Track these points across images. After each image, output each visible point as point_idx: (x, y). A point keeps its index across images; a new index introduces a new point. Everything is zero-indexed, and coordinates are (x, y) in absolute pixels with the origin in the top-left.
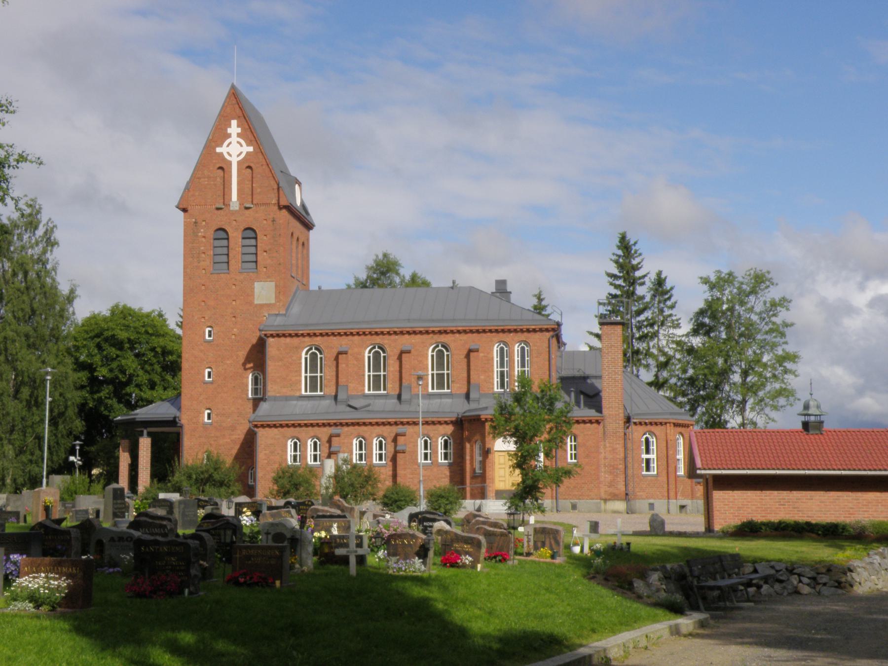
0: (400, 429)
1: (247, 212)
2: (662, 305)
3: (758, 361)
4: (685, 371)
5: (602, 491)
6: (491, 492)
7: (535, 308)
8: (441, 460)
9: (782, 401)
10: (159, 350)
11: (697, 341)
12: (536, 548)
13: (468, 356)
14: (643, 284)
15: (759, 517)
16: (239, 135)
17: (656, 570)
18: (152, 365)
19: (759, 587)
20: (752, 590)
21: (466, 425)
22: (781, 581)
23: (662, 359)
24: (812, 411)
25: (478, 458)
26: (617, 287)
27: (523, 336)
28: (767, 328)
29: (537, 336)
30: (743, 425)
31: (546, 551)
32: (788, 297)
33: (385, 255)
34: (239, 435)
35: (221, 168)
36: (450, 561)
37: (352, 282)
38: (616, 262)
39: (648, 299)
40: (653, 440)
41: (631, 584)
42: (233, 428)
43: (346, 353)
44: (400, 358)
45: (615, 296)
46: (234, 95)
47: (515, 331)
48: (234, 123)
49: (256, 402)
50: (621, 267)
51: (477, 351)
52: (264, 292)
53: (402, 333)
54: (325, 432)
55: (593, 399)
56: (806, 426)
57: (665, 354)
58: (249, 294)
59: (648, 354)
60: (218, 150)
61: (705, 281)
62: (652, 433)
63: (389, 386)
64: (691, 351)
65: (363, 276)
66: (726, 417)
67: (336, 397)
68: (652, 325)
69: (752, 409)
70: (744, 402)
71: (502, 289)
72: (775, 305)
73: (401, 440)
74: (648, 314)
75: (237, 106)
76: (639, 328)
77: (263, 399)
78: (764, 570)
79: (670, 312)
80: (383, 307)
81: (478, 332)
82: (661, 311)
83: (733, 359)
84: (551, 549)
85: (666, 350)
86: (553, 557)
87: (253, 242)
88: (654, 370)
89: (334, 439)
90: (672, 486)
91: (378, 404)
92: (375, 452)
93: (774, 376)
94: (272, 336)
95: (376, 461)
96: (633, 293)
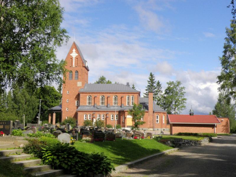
0: (107, 113)
1: (76, 68)
2: (159, 88)
3: (178, 100)
4: (163, 102)
5: (148, 126)
6: (126, 126)
7: (132, 88)
8: (116, 119)
9: (183, 108)
10: (54, 95)
11: (165, 95)
12: (147, 136)
13: (121, 98)
14: (155, 83)
15: (182, 132)
16: (75, 52)
17: (169, 140)
18: (53, 98)
19: (185, 144)
20: (184, 145)
21: (121, 112)
22: (189, 143)
23: (159, 99)
24: (192, 111)
25: (123, 119)
26: (149, 84)
27: (133, 94)
28: (180, 93)
29: (136, 94)
30: (175, 113)
31: (149, 137)
32: (185, 87)
33: (103, 76)
34: (74, 113)
35: (71, 58)
36: (135, 138)
37: (96, 82)
38: (150, 79)
39: (156, 86)
40: (158, 116)
41: (165, 143)
42: (72, 112)
43: (96, 97)
44: (107, 98)
45: (149, 86)
46: (74, 43)
47: (131, 93)
48: (74, 49)
49: (77, 107)
50: (150, 80)
51: (123, 97)
52: (79, 84)
53: (108, 93)
54: (92, 113)
55: (147, 107)
56: (190, 114)
57: (159, 98)
58: (76, 85)
59: (156, 98)
60: (71, 55)
61: (168, 83)
62: (158, 115)
63: (105, 104)
64: (164, 97)
65: (98, 81)
66: (171, 111)
67: (94, 106)
68: (157, 92)
69: (177, 110)
70: (175, 108)
71: (128, 84)
72: (182, 88)
73: (107, 115)
74: (156, 90)
75: (75, 46)
76: (59, 77)
77: (79, 106)
78: (186, 141)
79: (161, 89)
80: (102, 87)
81: (123, 93)
82: (159, 89)
83: (173, 99)
84: (150, 136)
85: (160, 97)
86: (150, 138)
87: (77, 74)
88: (157, 101)
89: (94, 115)
90: (162, 125)
91: (103, 108)
92: (89, 117)
93: (182, 103)
94: (81, 93)
95: (102, 119)
96: (153, 85)
